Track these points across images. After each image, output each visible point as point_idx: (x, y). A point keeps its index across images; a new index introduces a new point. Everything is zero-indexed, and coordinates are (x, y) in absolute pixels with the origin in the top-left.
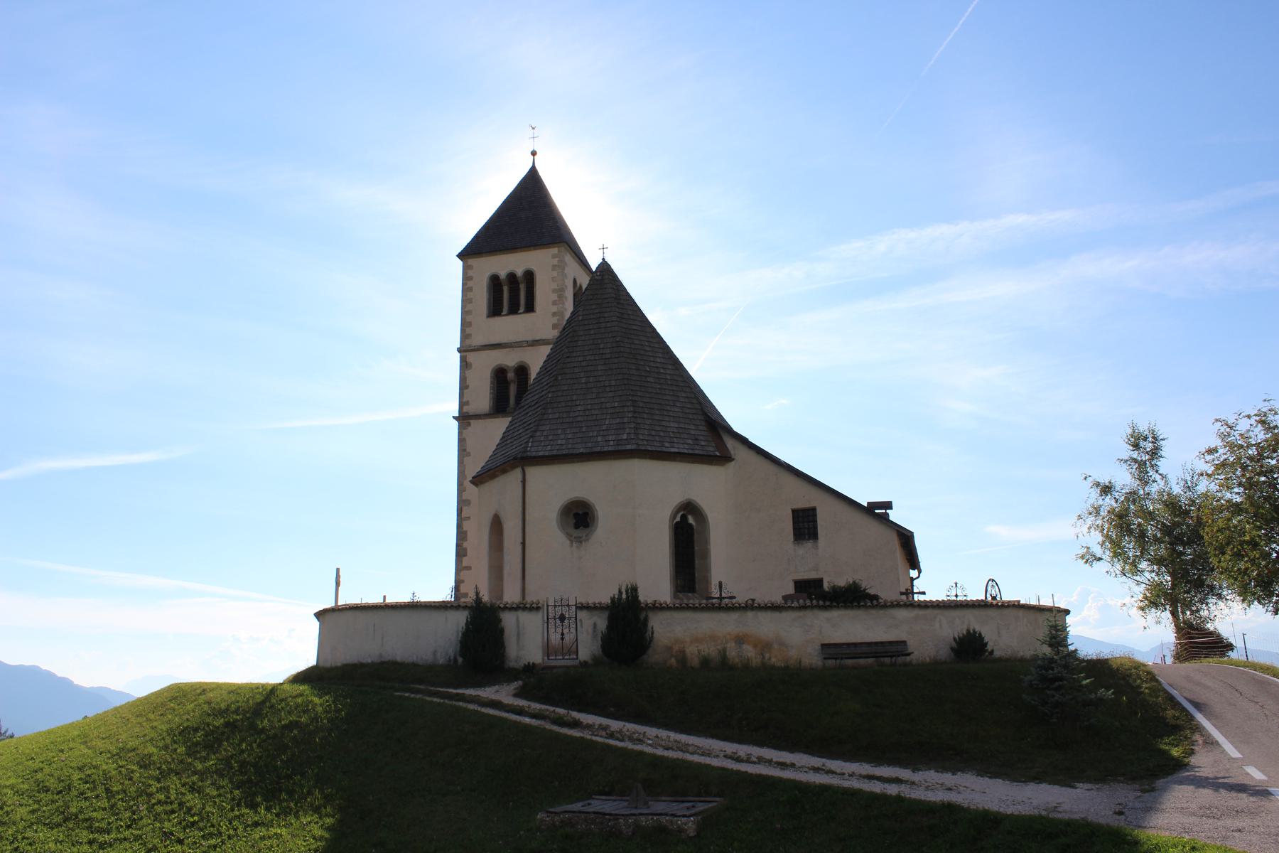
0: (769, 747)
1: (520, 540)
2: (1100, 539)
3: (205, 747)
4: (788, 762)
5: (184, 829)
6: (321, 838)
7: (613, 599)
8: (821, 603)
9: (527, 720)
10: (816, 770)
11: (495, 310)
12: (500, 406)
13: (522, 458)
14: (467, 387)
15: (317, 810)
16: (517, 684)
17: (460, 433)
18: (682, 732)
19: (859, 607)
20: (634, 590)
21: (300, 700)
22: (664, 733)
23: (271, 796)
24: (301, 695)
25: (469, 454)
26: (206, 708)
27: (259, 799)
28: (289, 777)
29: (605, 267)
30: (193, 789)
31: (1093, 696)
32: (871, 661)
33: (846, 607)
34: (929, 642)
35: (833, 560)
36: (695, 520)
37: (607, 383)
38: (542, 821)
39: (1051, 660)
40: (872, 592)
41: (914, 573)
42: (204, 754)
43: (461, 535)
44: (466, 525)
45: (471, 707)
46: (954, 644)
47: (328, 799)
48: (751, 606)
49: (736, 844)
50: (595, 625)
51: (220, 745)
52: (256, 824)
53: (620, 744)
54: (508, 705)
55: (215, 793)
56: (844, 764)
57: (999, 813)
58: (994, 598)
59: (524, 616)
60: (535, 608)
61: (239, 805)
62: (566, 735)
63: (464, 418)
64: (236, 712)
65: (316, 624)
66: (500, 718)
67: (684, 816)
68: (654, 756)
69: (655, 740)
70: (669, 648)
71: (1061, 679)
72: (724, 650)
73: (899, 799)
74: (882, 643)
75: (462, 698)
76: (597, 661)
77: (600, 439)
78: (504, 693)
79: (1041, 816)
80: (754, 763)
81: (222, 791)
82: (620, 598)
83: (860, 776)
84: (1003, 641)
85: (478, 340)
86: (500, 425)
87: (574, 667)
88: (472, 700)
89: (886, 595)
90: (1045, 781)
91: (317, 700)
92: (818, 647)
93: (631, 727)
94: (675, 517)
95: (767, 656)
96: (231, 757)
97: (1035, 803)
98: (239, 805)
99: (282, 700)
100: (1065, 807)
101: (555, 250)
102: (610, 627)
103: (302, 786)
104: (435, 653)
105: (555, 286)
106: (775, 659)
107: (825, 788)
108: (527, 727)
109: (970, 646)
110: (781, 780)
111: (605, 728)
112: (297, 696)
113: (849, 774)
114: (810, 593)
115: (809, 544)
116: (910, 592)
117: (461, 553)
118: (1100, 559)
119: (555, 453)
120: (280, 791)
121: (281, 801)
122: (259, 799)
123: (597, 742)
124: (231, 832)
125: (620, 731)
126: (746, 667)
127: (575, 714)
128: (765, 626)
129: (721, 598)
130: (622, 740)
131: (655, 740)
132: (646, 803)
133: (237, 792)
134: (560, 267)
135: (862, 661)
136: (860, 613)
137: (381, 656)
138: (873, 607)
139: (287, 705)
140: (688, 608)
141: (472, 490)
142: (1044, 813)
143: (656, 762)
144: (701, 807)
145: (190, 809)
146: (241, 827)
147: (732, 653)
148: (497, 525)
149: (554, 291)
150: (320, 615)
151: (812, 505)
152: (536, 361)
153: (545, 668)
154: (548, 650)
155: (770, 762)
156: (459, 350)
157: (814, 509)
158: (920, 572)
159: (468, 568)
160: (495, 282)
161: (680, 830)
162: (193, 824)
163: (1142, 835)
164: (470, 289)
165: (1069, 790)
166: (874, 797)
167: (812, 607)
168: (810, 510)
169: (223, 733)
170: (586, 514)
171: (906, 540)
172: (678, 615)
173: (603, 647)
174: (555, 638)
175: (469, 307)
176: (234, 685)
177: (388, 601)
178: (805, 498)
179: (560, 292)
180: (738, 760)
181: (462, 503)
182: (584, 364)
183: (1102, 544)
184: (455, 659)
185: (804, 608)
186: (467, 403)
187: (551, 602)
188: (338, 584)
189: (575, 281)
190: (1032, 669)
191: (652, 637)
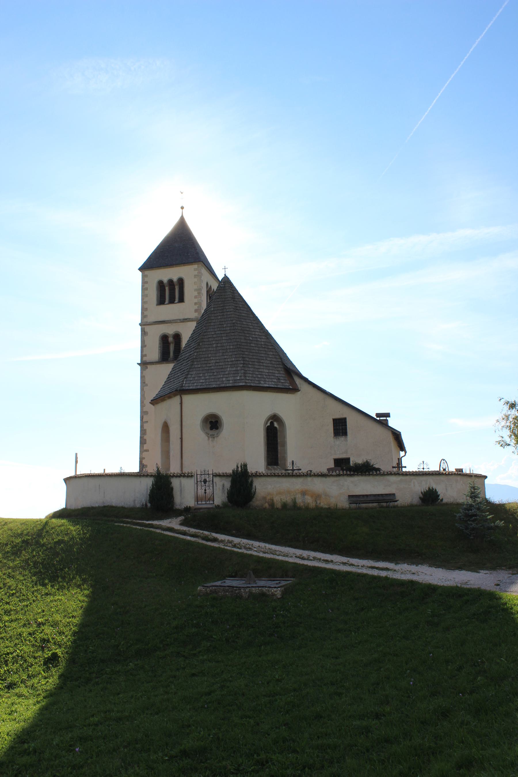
0: (319, 552)
1: (179, 436)
2: (509, 433)
3: (13, 554)
4: (329, 559)
5: (9, 597)
6: (83, 601)
7: (233, 471)
8: (348, 473)
9: (189, 538)
10: (344, 564)
11: (161, 301)
12: (164, 358)
13: (180, 390)
14: (145, 346)
15: (79, 586)
16: (182, 518)
17: (142, 373)
18: (272, 544)
19: (369, 475)
20: (245, 466)
21: (63, 528)
22: (262, 545)
23: (53, 579)
24: (62, 525)
25: (147, 385)
26: (9, 532)
27: (47, 581)
28: (61, 570)
29: (226, 279)
30: (9, 577)
31: (492, 524)
32: (375, 504)
33: (362, 475)
34: (407, 494)
35: (357, 447)
36: (278, 424)
37: (228, 347)
38: (200, 591)
39: (471, 506)
40: (376, 466)
41: (402, 453)
42: (12, 558)
43: (143, 432)
44: (146, 426)
45: (158, 531)
46: (421, 496)
47: (84, 581)
48: (309, 474)
49: (302, 602)
50: (223, 485)
51: (21, 553)
52: (47, 594)
53: (240, 551)
54: (178, 530)
55: (22, 578)
56: (359, 560)
57: (436, 585)
58: (444, 470)
59: (184, 480)
60: (190, 476)
61: (36, 584)
62: (210, 546)
63: (144, 364)
64: (27, 534)
65: (64, 486)
66: (174, 537)
67: (275, 587)
68: (258, 557)
69: (258, 548)
70: (264, 498)
71: (476, 515)
72: (295, 499)
73: (386, 578)
74: (382, 495)
75: (152, 526)
76: (225, 505)
77: (224, 379)
78: (174, 523)
79: (457, 587)
80: (311, 560)
81: (26, 577)
82: (237, 470)
83: (368, 567)
84: (449, 493)
85: (151, 319)
86: (167, 368)
87: (212, 508)
88: (158, 527)
89: (385, 467)
90: (464, 570)
91: (72, 528)
92: (347, 497)
93: (245, 541)
94: (267, 423)
95: (318, 502)
96: (28, 559)
97: (457, 580)
98: (36, 584)
99: (52, 528)
100: (472, 582)
101: (195, 266)
102: (232, 487)
103: (69, 574)
104: (134, 501)
105: (196, 287)
106: (323, 504)
107: (349, 573)
108: (189, 542)
109: (430, 497)
110: (325, 569)
111: (231, 542)
112: (60, 526)
113: (362, 566)
114: (343, 466)
115: (342, 438)
116: (399, 465)
117: (143, 442)
118: (509, 445)
119: (199, 387)
120: (58, 577)
121: (59, 583)
122: (47, 581)
123: (227, 550)
124: (34, 598)
125: (239, 544)
126: (307, 508)
127: (215, 535)
128: (318, 485)
129: (293, 470)
130: (240, 549)
131: (258, 548)
132: (255, 581)
133: (34, 578)
134: (199, 276)
135: (371, 505)
136: (371, 478)
137: (103, 503)
138: (377, 475)
139: (56, 531)
140: (275, 476)
141: (150, 408)
142: (459, 585)
143: (260, 560)
144: (283, 583)
145: (10, 587)
146: (39, 596)
147: (299, 501)
148: (166, 428)
149: (195, 290)
150: (67, 480)
151: (344, 416)
152: (187, 332)
153: (195, 509)
154: (197, 499)
155: (320, 560)
156: (140, 325)
157: (345, 419)
158: (406, 453)
159: (147, 451)
160: (161, 285)
161: (273, 595)
162: (13, 594)
163: (504, 595)
164: (147, 289)
165: (475, 574)
166: (374, 577)
167: (343, 475)
168: (343, 420)
169: (22, 547)
170: (217, 422)
171: (397, 436)
172: (269, 479)
173: (228, 497)
174: (201, 492)
175: (146, 299)
176: (23, 520)
177: (107, 472)
178: (340, 413)
179: (199, 290)
180: (303, 559)
181: (143, 414)
182: (215, 336)
183: (510, 436)
184: (146, 505)
185: (339, 475)
186: (145, 355)
187: (199, 473)
188: (76, 462)
189: (207, 284)
190: (461, 510)
191: (255, 492)
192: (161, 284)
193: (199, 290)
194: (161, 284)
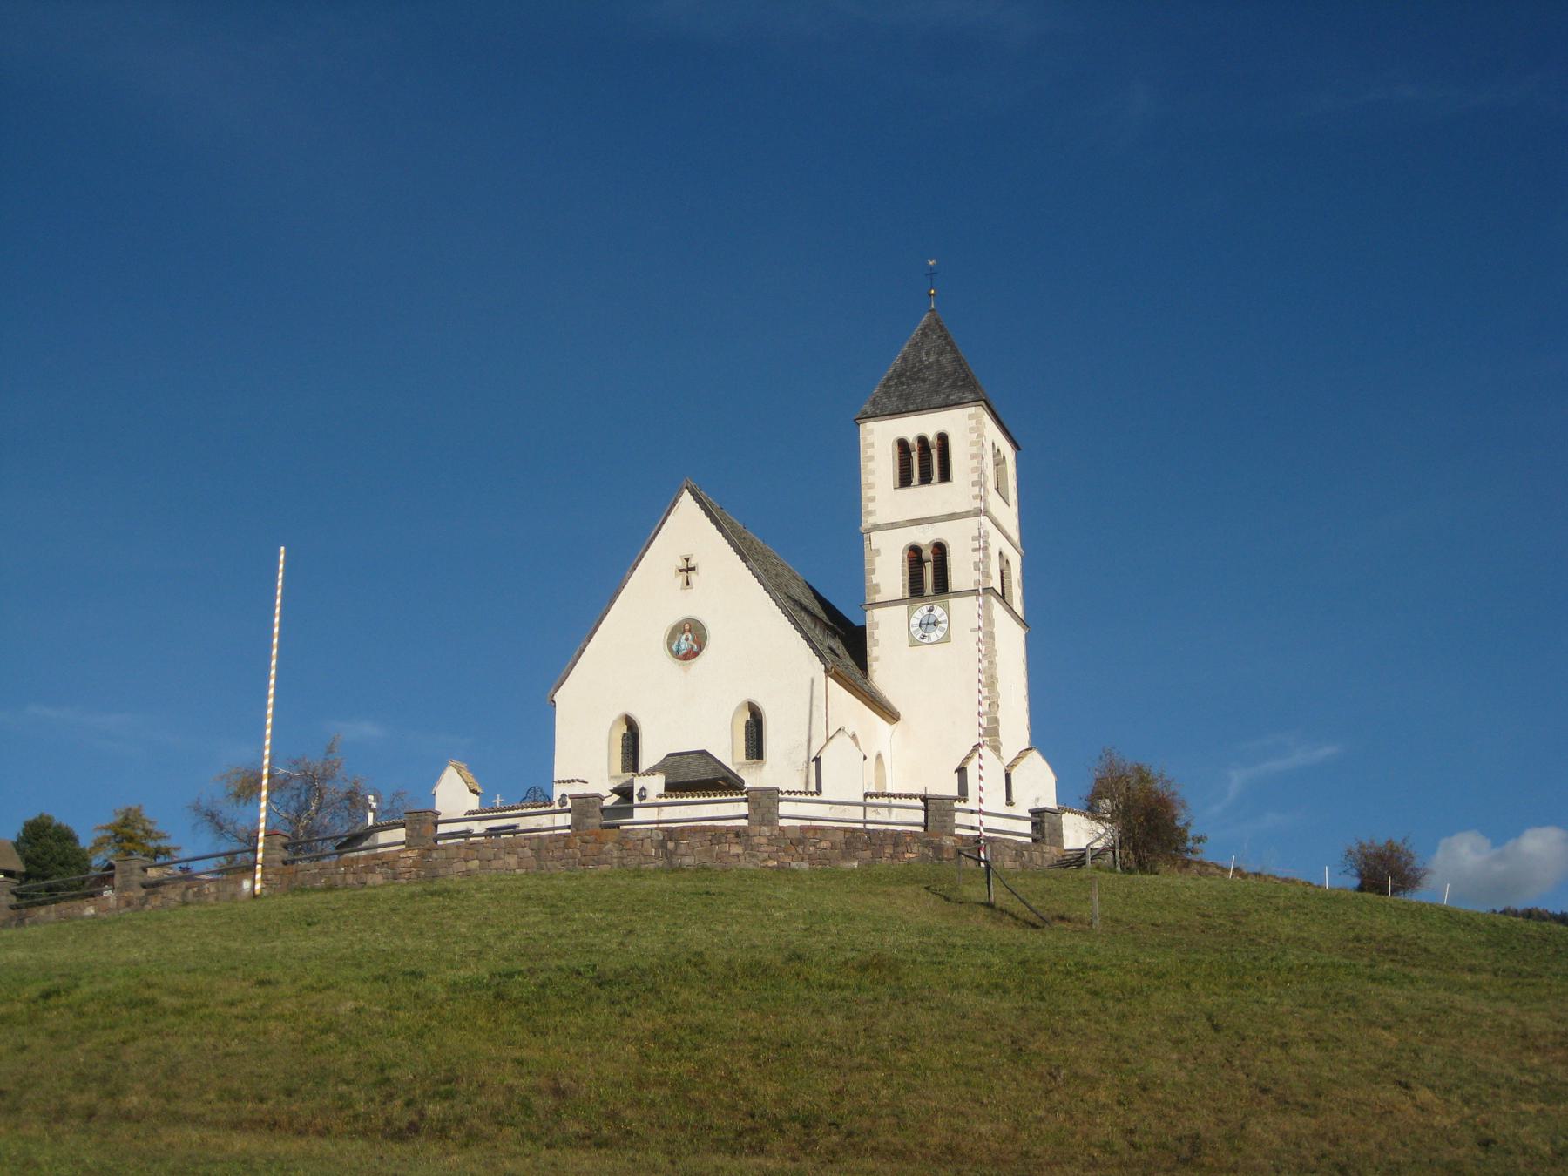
20: (194, 827)
101: (971, 410)
192: (903, 445)
193: (978, 457)
194: (903, 445)
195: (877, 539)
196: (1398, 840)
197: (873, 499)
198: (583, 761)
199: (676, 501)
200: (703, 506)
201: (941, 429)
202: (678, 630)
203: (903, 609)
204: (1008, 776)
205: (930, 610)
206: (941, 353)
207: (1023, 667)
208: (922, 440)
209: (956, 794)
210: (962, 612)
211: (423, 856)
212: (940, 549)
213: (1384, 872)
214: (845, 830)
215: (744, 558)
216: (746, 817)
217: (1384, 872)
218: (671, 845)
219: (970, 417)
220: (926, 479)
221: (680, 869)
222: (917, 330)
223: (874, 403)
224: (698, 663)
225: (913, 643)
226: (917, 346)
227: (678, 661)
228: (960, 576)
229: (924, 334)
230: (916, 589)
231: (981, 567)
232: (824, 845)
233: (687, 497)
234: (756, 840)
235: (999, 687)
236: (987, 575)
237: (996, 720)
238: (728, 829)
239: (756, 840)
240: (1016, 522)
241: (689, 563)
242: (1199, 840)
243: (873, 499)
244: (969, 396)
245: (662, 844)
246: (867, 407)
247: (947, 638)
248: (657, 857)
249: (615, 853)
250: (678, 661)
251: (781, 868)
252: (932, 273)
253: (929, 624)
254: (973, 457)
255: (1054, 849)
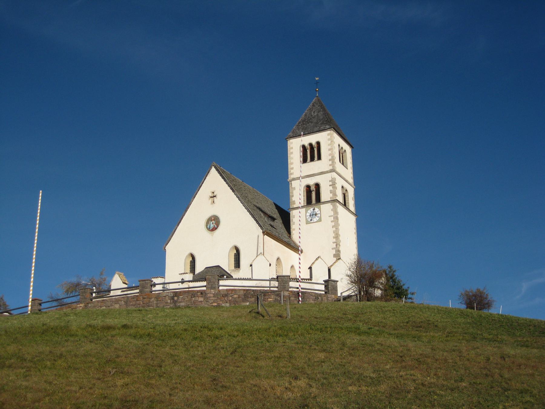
101: (329, 132)
192: (304, 147)
194: (304, 147)
195: (294, 184)
196: (482, 289)
197: (292, 168)
198: (175, 273)
199: (209, 171)
200: (219, 172)
201: (317, 140)
202: (210, 220)
203: (303, 210)
204: (329, 270)
205: (314, 210)
206: (319, 112)
207: (355, 231)
208: (311, 145)
209: (309, 277)
210: (326, 209)
211: (86, 306)
212: (317, 186)
213: (477, 301)
214: (244, 290)
215: (233, 191)
216: (205, 286)
217: (477, 301)
218: (176, 298)
219: (328, 135)
220: (312, 159)
221: (179, 307)
222: (311, 104)
223: (293, 132)
224: (217, 232)
225: (307, 223)
226: (311, 110)
227: (213, 235)
228: (325, 195)
229: (313, 105)
230: (309, 202)
231: (334, 193)
232: (235, 296)
233: (213, 170)
234: (209, 295)
235: (340, 238)
236: (335, 195)
237: (339, 251)
238: (198, 291)
239: (209, 295)
240: (352, 175)
241: (215, 195)
242: (413, 294)
243: (292, 168)
244: (328, 127)
245: (172, 298)
246: (291, 134)
247: (320, 220)
248: (170, 303)
249: (155, 302)
250: (213, 235)
251: (219, 306)
252: (317, 82)
253: (314, 215)
254: (329, 150)
255: (333, 296)
